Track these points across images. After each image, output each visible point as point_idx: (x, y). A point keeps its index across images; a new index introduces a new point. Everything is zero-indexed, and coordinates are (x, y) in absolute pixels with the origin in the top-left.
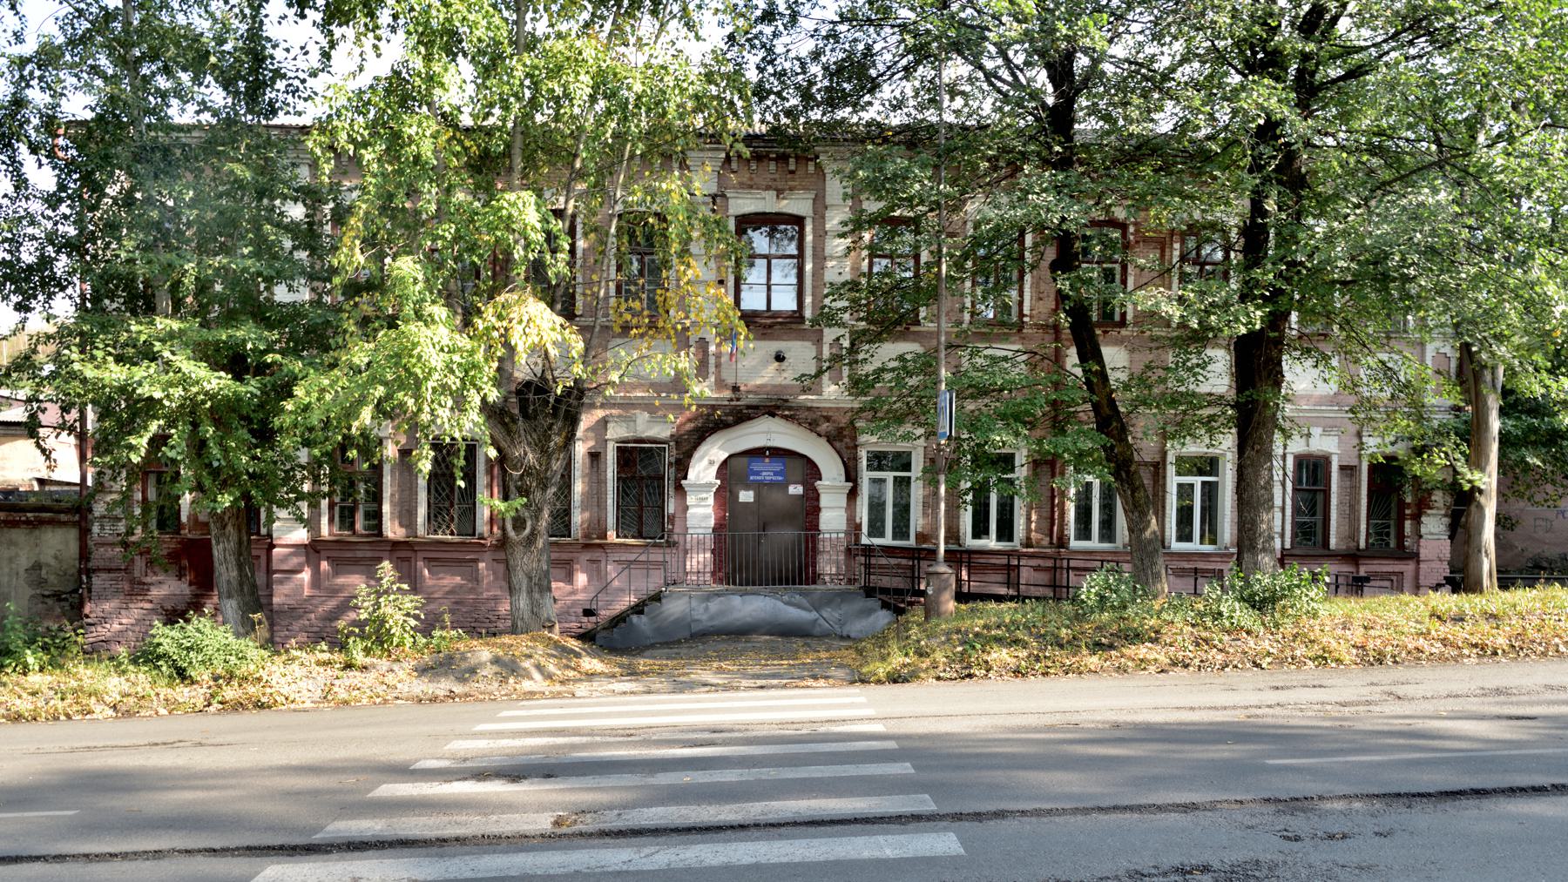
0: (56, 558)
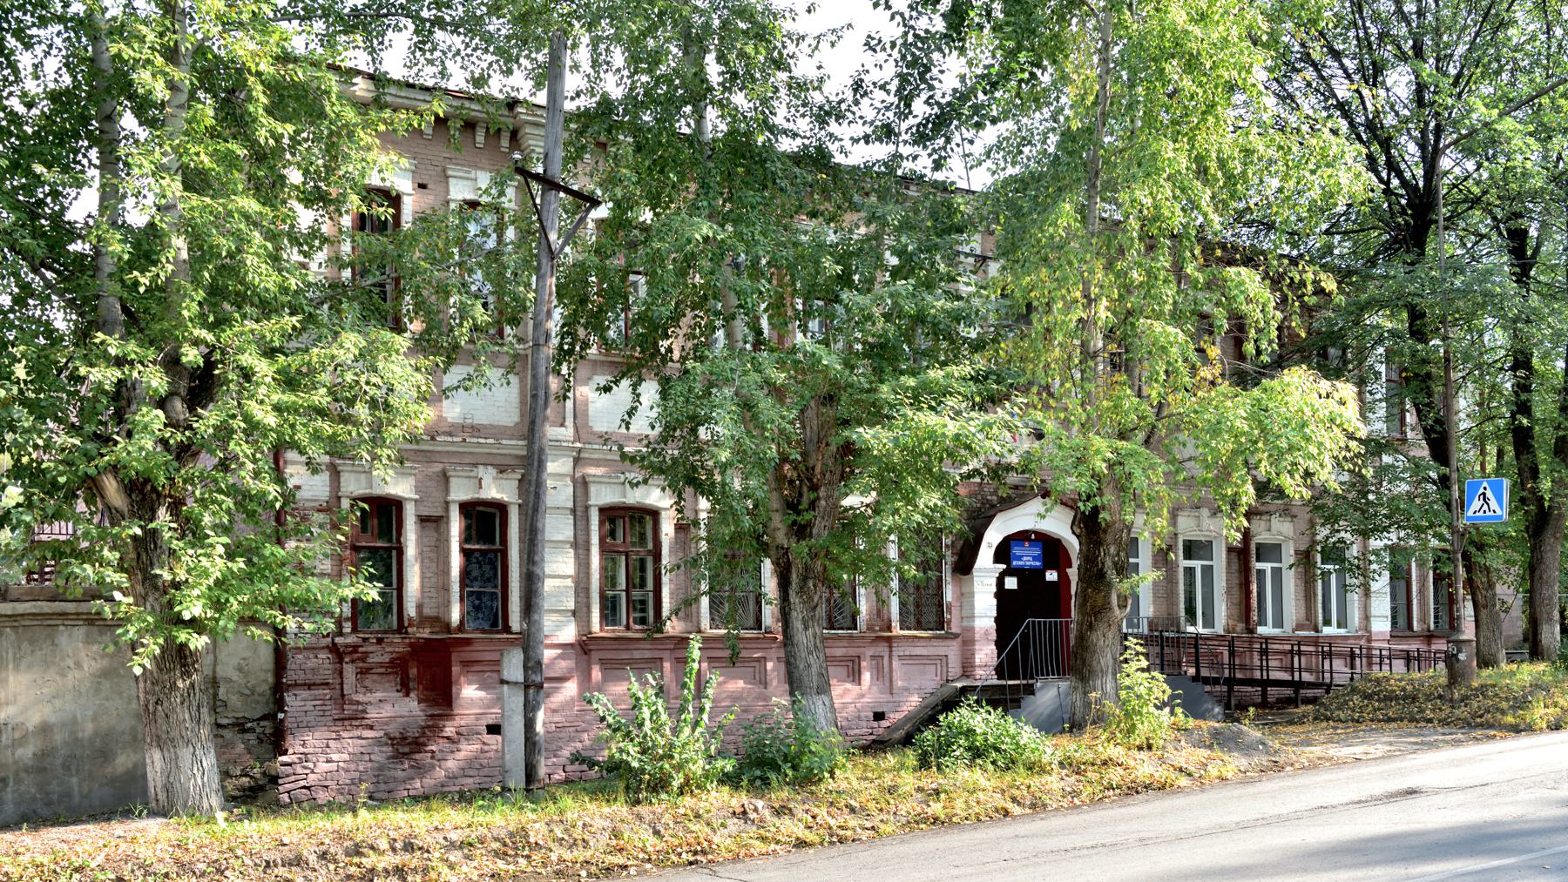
0: (240, 669)
